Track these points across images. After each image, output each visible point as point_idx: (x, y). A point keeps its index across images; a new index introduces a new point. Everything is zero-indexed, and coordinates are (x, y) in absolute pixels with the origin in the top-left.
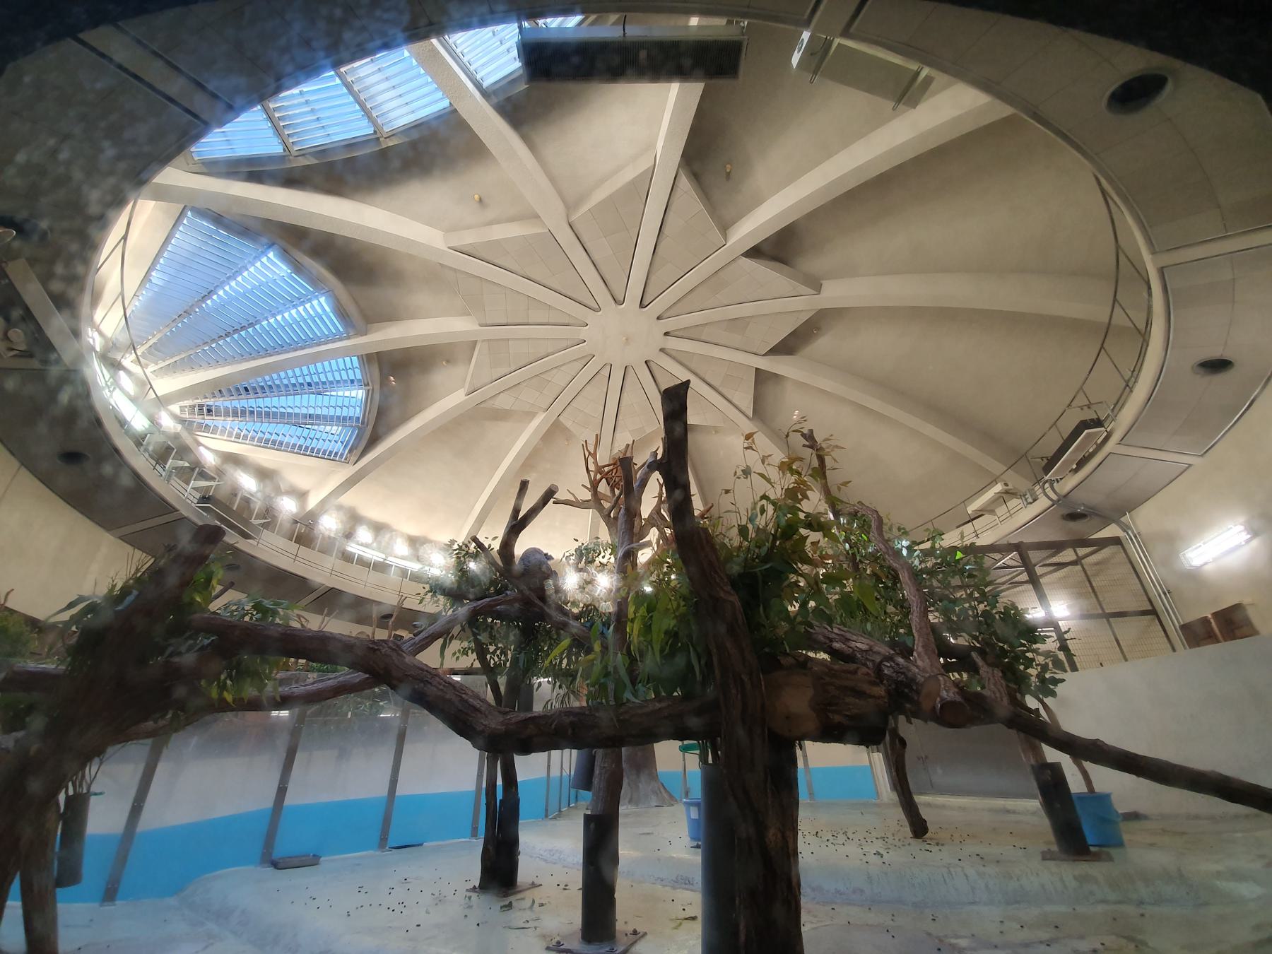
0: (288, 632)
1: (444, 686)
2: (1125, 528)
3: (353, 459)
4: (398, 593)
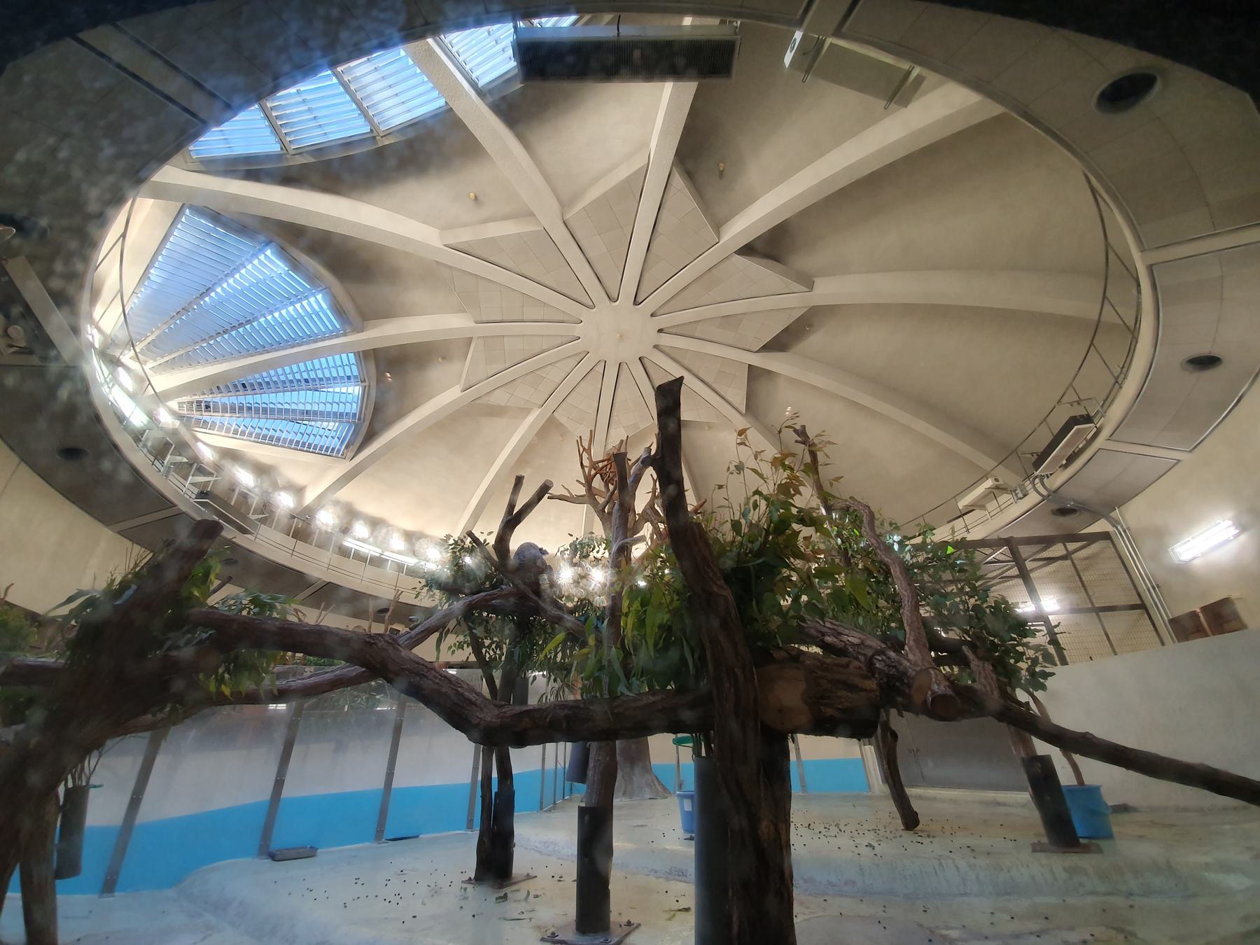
0: (286, 626)
1: (440, 679)
2: (1115, 523)
3: (350, 454)
4: (394, 588)
